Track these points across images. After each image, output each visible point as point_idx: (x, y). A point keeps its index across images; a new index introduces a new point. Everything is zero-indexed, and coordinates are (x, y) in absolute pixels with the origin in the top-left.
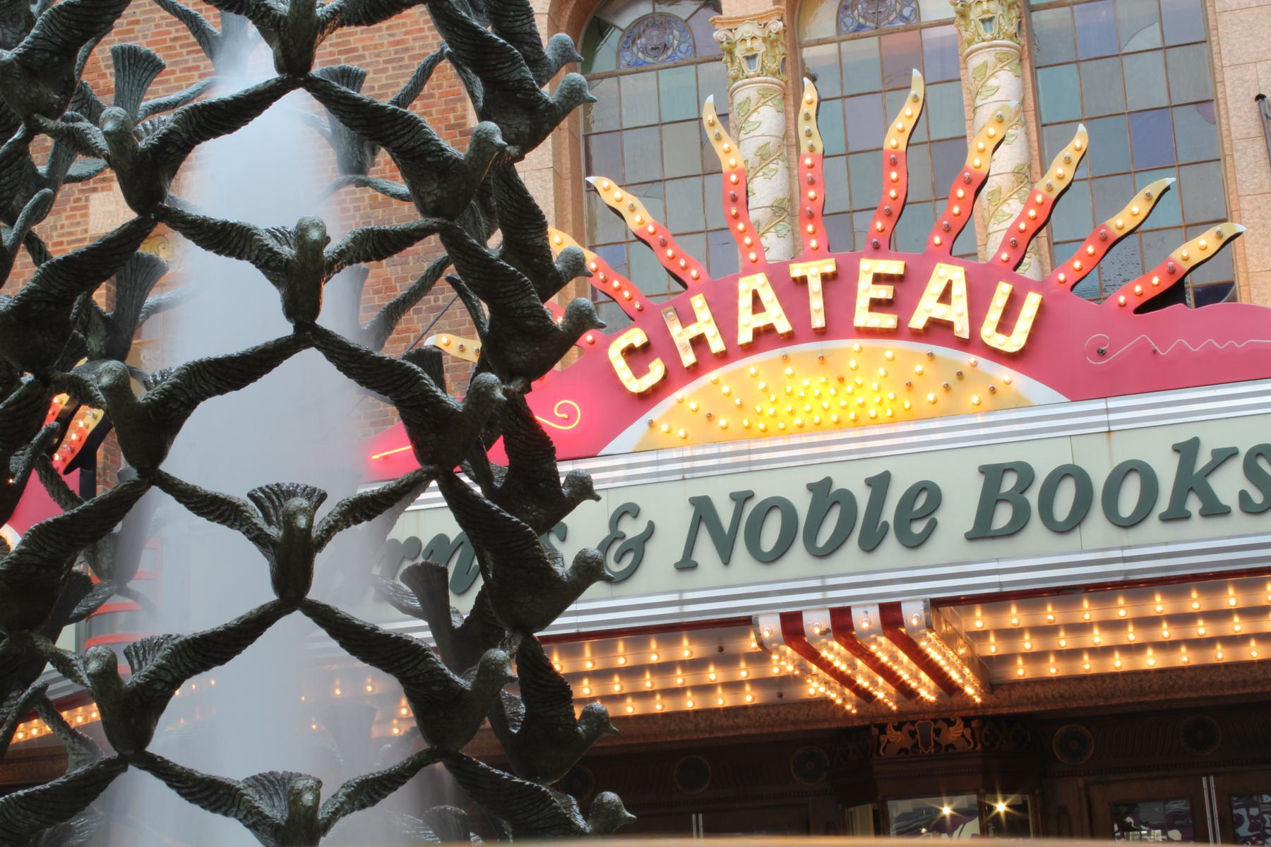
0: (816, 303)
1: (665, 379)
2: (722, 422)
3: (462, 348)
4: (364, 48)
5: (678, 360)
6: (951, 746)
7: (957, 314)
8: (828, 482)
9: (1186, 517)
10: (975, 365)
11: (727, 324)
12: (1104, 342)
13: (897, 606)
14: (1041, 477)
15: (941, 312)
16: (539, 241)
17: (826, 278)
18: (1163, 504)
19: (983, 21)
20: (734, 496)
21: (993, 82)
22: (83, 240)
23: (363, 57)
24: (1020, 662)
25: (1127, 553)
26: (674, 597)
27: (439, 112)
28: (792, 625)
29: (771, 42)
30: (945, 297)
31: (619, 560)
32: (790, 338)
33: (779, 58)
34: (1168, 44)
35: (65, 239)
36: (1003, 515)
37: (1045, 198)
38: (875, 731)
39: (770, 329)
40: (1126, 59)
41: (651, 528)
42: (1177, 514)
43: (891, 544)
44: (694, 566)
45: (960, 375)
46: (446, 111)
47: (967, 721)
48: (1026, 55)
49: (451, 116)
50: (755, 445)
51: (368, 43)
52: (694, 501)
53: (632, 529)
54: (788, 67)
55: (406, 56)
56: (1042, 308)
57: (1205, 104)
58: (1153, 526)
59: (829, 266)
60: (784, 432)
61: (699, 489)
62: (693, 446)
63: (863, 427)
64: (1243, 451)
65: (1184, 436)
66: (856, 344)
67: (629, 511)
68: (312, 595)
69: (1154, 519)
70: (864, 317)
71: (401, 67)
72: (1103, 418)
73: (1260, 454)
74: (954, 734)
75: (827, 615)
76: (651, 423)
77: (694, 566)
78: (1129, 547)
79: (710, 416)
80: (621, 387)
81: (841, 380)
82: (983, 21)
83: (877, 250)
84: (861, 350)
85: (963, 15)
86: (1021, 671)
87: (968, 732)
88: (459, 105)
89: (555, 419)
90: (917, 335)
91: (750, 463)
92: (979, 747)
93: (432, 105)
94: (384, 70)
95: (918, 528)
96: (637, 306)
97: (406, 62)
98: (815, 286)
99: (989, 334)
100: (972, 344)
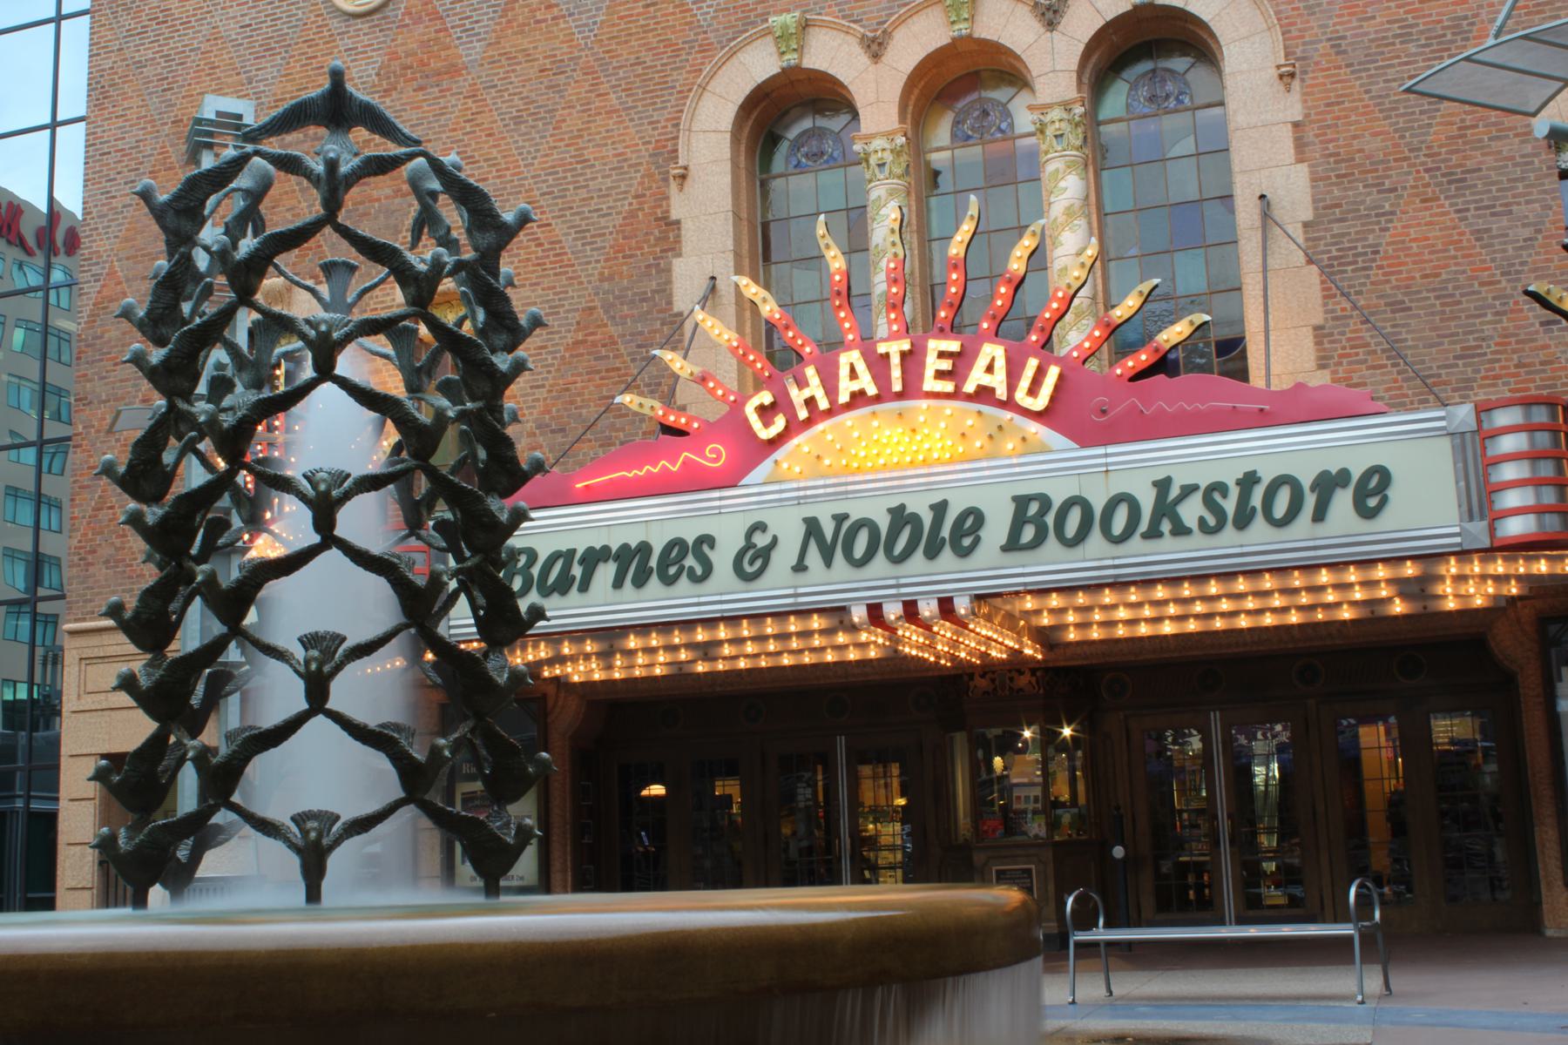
0: (896, 373)
1: (786, 428)
2: (827, 462)
3: (641, 405)
4: (595, 159)
5: (796, 416)
6: (1021, 690)
7: (998, 381)
8: (902, 507)
9: (1160, 535)
10: (1012, 419)
11: (831, 389)
12: (1104, 403)
13: (950, 600)
14: (1056, 504)
15: (987, 380)
16: (509, 453)
17: (903, 355)
18: (1144, 526)
19: (1056, 136)
20: (835, 517)
21: (1062, 184)
22: (392, 307)
23: (593, 166)
24: (1072, 629)
25: (1117, 562)
26: (791, 591)
27: (650, 208)
28: (875, 613)
29: (897, 153)
30: (990, 369)
31: (751, 563)
32: (878, 399)
33: (904, 165)
34: (1201, 151)
35: (379, 306)
36: (1028, 533)
37: (1065, 294)
38: (966, 678)
39: (862, 393)
40: (1168, 163)
41: (775, 540)
42: (1153, 533)
43: (947, 554)
44: (805, 569)
45: (1000, 428)
46: (655, 207)
47: (1033, 671)
48: (1090, 161)
49: (659, 211)
50: (850, 479)
51: (597, 155)
52: (806, 520)
53: (761, 540)
54: (911, 170)
55: (625, 165)
56: (1061, 377)
57: (1227, 198)
58: (1136, 542)
59: (906, 345)
60: (874, 470)
61: (809, 512)
62: (806, 479)
63: (930, 466)
64: (1203, 486)
65: (1160, 476)
66: (924, 404)
67: (760, 527)
68: (329, 706)
69: (1137, 536)
70: (930, 384)
71: (622, 174)
72: (1103, 460)
73: (1214, 489)
74: (1023, 681)
75: (900, 606)
76: (776, 462)
77: (805, 569)
78: (1118, 558)
79: (818, 457)
80: (754, 436)
81: (914, 431)
82: (1056, 136)
83: (942, 333)
84: (929, 407)
85: (1042, 132)
86: (1072, 636)
87: (1033, 680)
88: (664, 203)
89: (705, 458)
90: (969, 398)
91: (847, 492)
92: (1041, 691)
93: (645, 202)
94: (609, 176)
95: (967, 542)
96: (767, 374)
97: (626, 169)
98: (895, 360)
99: (1021, 396)
100: (1009, 404)
